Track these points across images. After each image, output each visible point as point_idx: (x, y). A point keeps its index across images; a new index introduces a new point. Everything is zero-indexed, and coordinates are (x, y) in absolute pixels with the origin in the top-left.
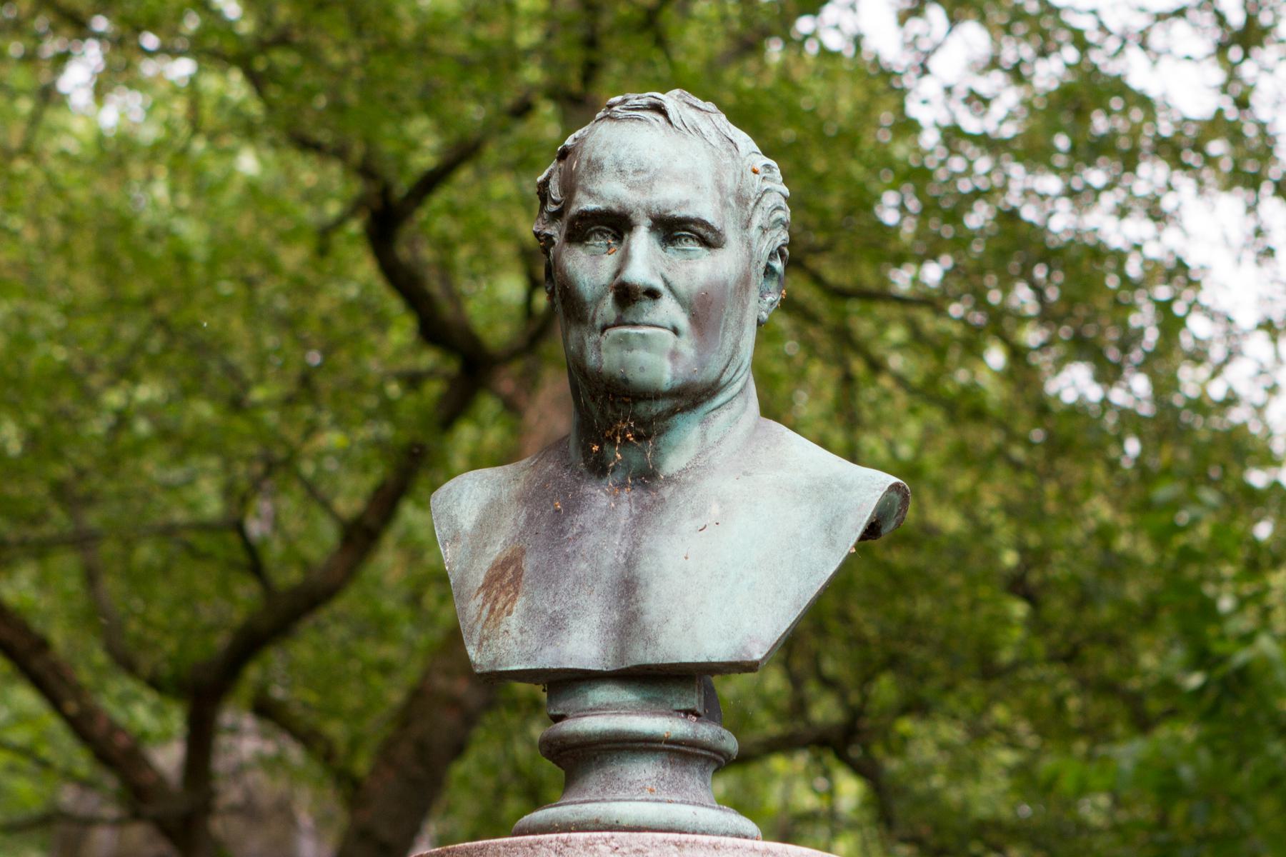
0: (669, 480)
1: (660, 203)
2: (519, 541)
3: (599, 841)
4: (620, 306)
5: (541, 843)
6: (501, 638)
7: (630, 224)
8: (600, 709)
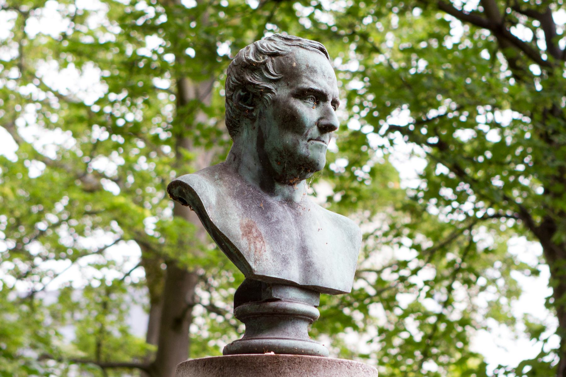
4: (321, 133)
5: (343, 363)
6: (265, 261)
7: (326, 99)
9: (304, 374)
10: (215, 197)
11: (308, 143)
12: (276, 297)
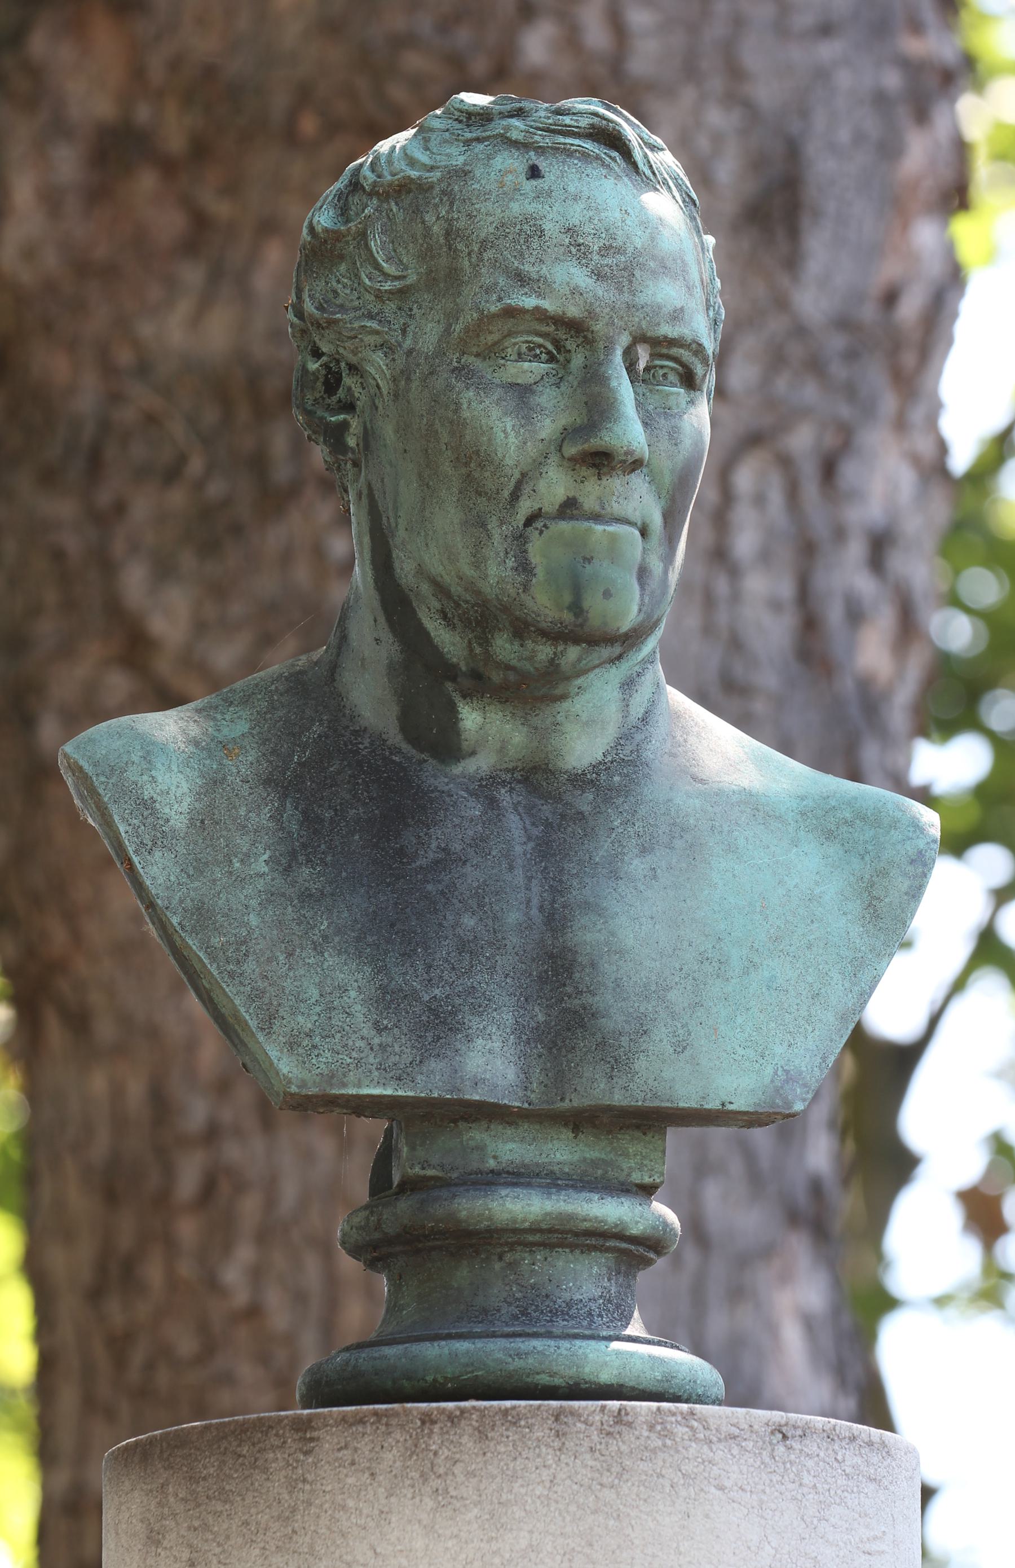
12: (422, 1173)
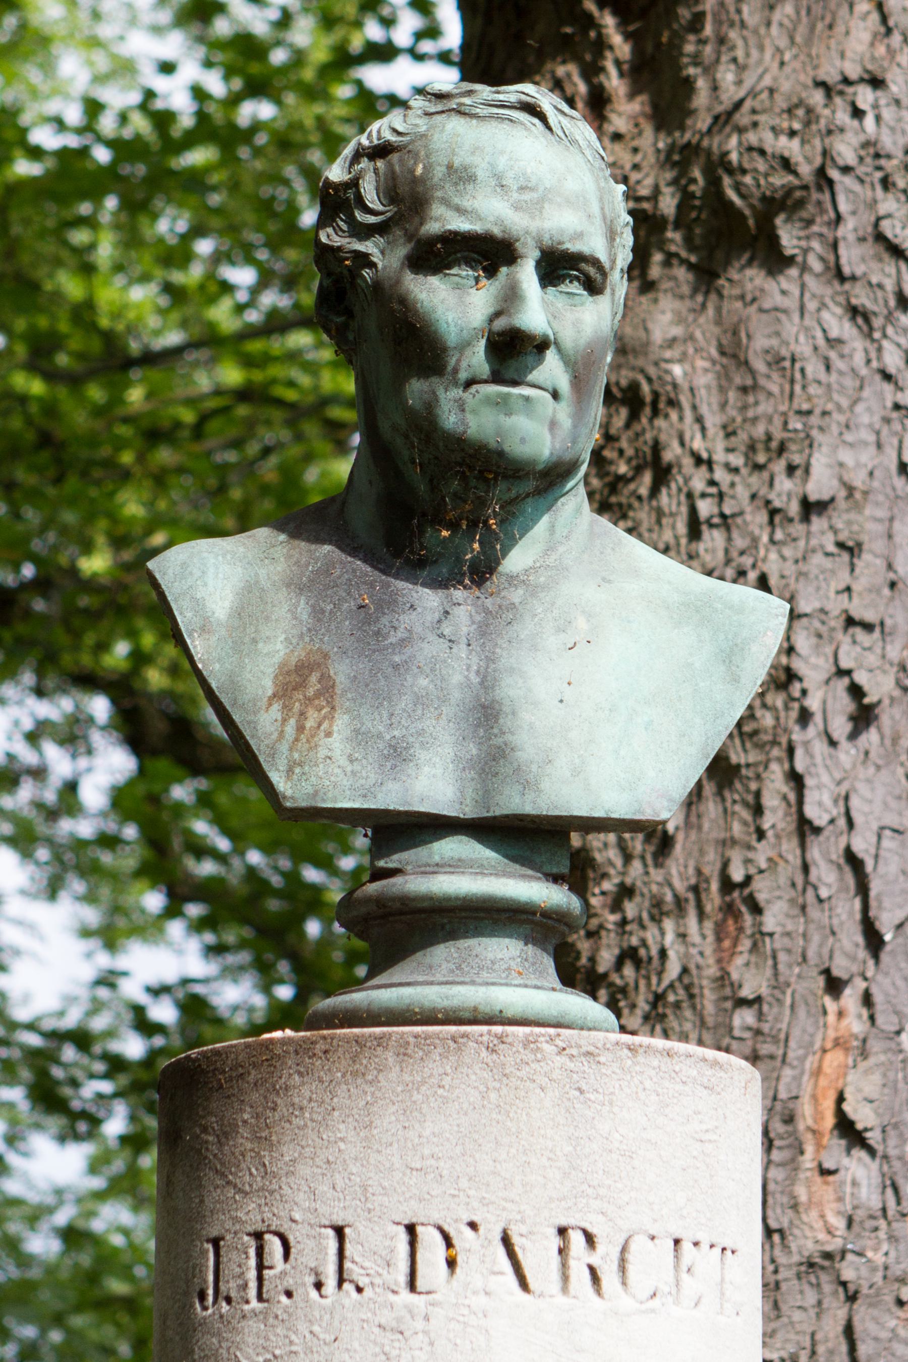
0: (512, 579)
1: (554, 232)
2: (312, 640)
3: (542, 1039)
6: (321, 766)
8: (450, 866)
9: (339, 1084)
10: (230, 597)
11: (467, 396)
